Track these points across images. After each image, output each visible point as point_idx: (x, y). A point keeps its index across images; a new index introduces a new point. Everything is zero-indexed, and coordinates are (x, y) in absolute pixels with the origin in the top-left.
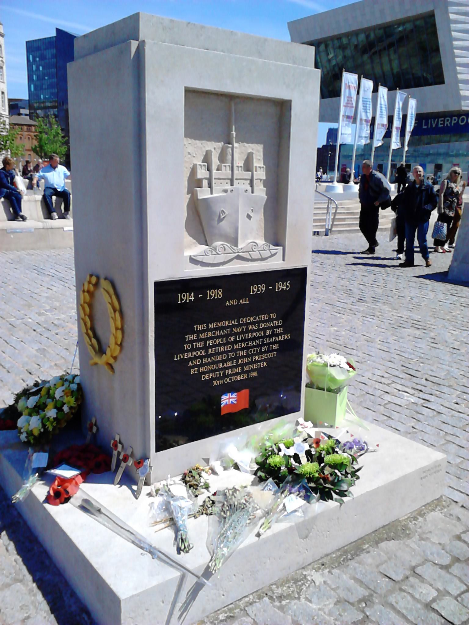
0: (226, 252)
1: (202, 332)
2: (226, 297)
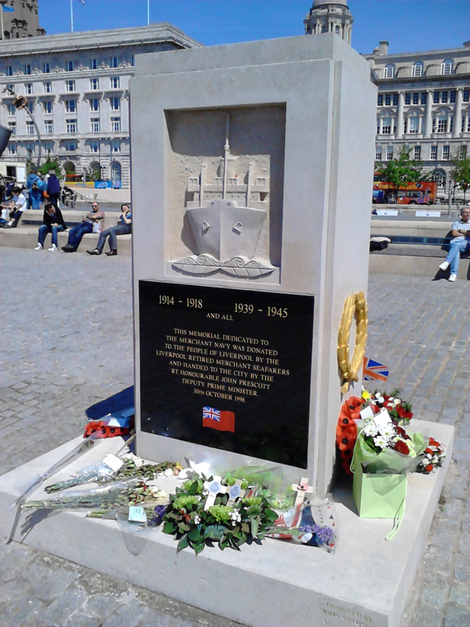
0: (206, 264)
1: (183, 336)
2: (206, 309)
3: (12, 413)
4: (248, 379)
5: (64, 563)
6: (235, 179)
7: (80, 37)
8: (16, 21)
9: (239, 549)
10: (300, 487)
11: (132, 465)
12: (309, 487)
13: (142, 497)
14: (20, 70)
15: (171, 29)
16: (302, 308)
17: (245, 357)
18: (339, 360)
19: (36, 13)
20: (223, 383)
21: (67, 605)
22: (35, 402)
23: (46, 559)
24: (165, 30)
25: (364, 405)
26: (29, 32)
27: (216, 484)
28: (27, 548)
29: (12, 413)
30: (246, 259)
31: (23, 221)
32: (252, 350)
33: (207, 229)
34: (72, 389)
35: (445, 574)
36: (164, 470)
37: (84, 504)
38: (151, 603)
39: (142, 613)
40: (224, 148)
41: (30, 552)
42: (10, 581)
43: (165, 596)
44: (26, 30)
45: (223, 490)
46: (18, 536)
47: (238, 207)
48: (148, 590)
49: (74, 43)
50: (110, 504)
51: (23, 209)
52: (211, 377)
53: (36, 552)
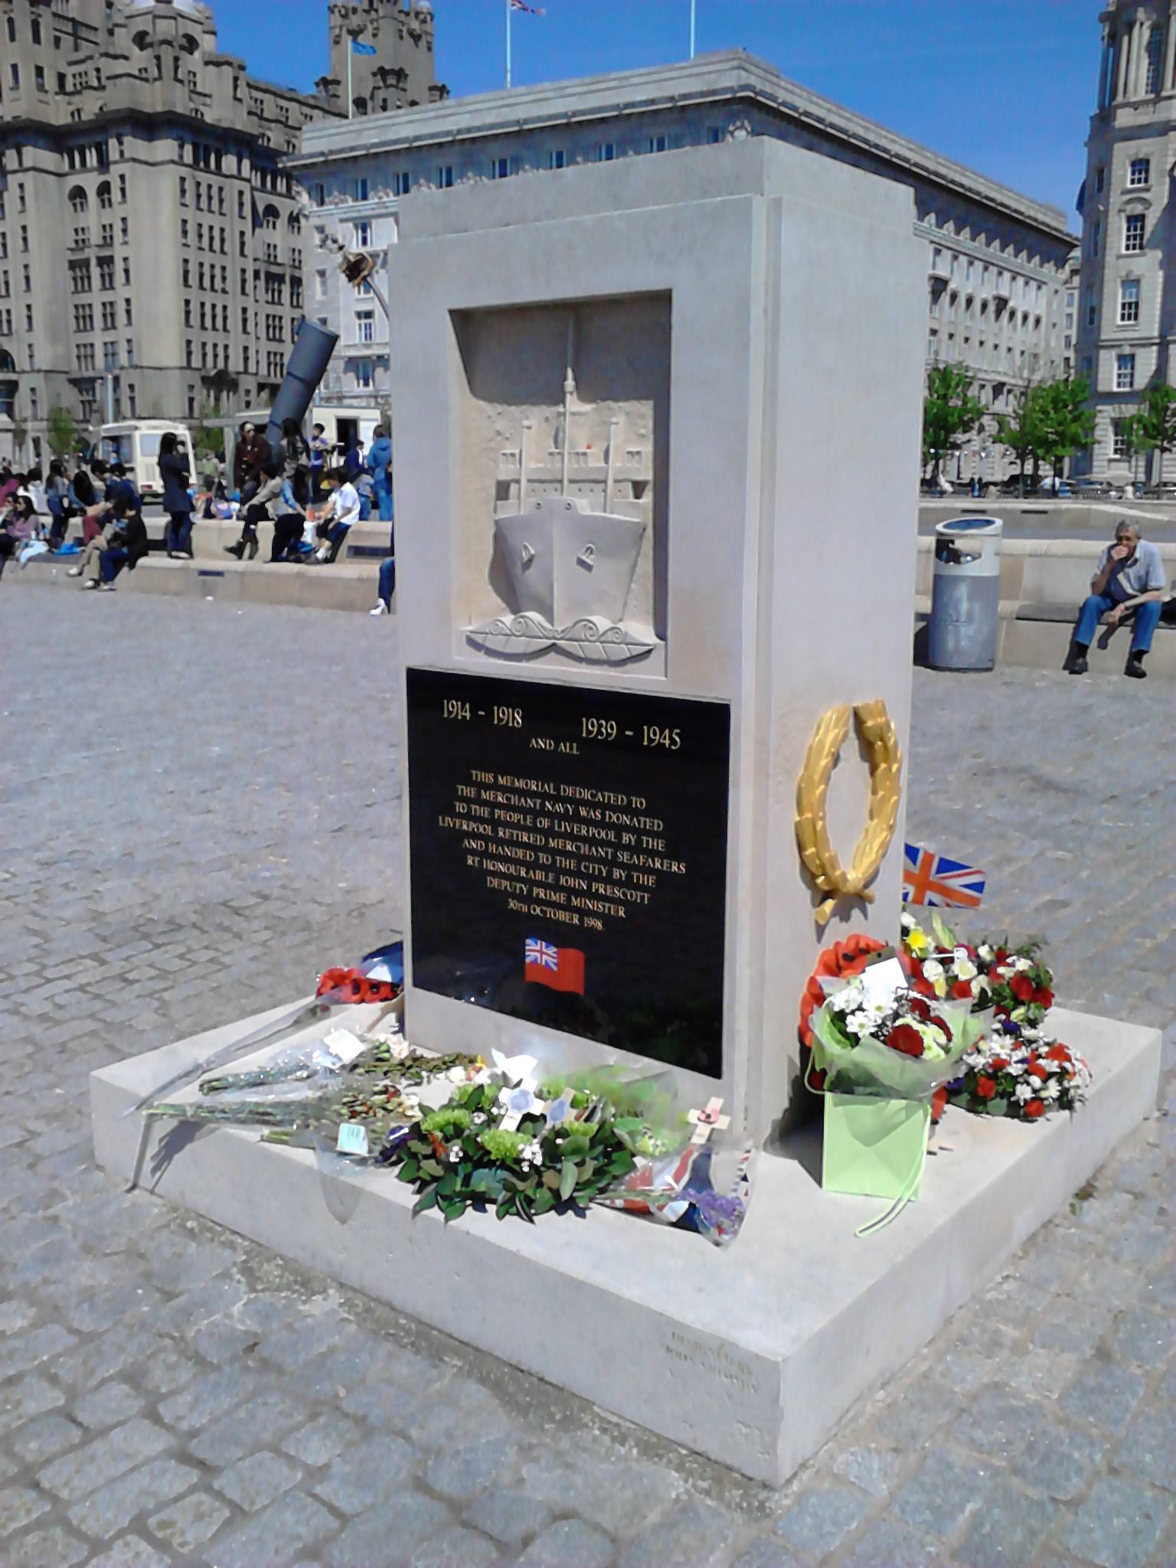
1: (487, 787)
3: (211, 954)
4: (608, 880)
5: (221, 1234)
6: (585, 454)
7: (526, 99)
8: (383, 72)
9: (532, 1221)
10: (703, 1117)
11: (386, 1055)
12: (722, 1117)
13: (380, 1113)
14: (386, 186)
15: (747, 66)
16: (706, 726)
17: (603, 834)
18: (801, 848)
19: (429, 49)
20: (562, 889)
21: (205, 1304)
22: (265, 935)
23: (189, 1224)
24: (733, 68)
25: (879, 955)
26: (411, 95)
27: (525, 1094)
28: (159, 1201)
29: (211, 954)
30: (602, 623)
31: (350, 547)
32: (614, 818)
33: (530, 560)
34: (349, 914)
35: (1010, 1332)
36: (448, 1068)
37: (259, 1116)
38: (365, 1320)
39: (339, 1333)
40: (563, 386)
41: (164, 1210)
42: (115, 1254)
43: (393, 1309)
44: (404, 90)
45: (537, 1108)
46: (146, 1180)
47: (588, 512)
48: (365, 1295)
49: (511, 115)
50: (311, 1122)
51: (351, 519)
52: (539, 875)
53: (175, 1210)
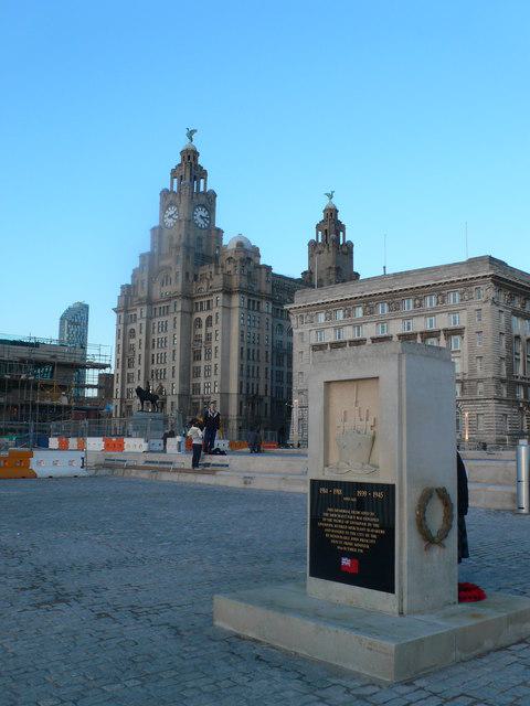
52: (346, 538)
